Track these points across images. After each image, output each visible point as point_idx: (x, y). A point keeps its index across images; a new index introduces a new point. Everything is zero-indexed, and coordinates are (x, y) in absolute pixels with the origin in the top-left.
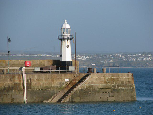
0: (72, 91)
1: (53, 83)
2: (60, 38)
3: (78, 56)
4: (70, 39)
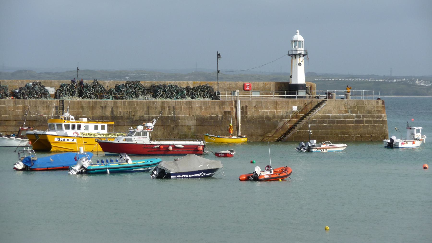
0: (311, 113)
1: (277, 111)
2: (290, 54)
3: (421, 81)
4: (304, 56)
